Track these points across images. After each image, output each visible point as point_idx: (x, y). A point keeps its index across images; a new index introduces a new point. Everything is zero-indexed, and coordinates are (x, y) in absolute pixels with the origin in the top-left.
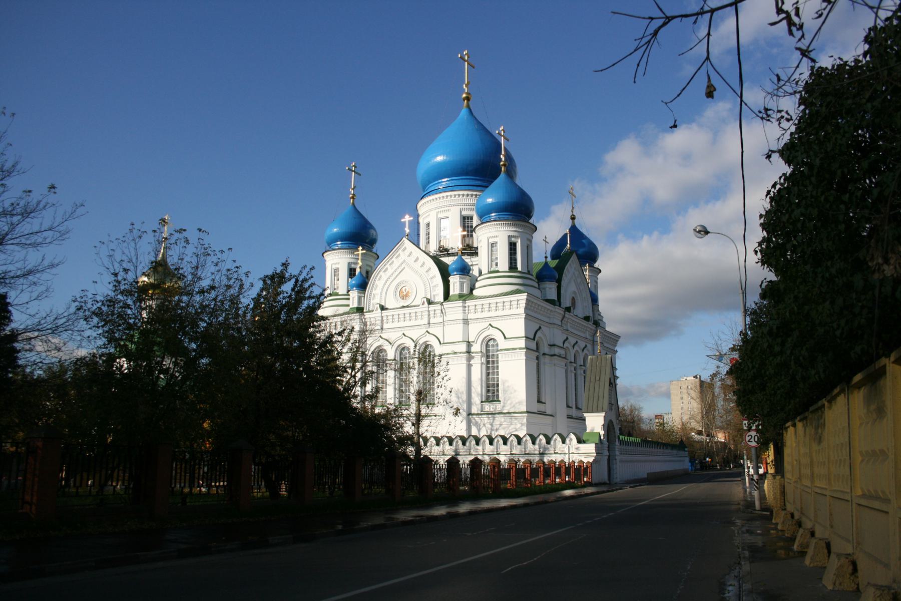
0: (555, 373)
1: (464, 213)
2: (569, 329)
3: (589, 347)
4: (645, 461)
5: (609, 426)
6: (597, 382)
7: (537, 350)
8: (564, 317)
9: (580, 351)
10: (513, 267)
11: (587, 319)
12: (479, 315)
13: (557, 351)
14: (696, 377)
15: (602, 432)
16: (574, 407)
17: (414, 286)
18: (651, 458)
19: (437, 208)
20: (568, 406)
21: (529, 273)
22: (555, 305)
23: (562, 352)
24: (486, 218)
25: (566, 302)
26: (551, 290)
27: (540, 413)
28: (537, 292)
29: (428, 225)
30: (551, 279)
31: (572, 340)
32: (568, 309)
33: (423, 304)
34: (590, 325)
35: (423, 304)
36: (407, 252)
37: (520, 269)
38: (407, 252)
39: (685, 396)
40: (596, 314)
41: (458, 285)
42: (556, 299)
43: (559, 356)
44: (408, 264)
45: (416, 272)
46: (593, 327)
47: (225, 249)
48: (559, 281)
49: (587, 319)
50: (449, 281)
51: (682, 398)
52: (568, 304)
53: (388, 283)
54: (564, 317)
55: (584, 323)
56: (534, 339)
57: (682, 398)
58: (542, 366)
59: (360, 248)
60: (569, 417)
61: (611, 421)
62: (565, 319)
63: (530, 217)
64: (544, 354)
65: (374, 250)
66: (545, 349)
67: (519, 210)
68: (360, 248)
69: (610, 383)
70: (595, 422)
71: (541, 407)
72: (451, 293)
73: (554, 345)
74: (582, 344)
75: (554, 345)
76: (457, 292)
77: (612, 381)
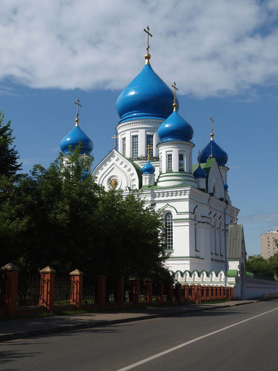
0: (204, 232)
3: (223, 217)
5: (241, 267)
8: (210, 199)
9: (218, 219)
10: (181, 170)
11: (221, 199)
12: (161, 198)
13: (205, 220)
16: (219, 255)
17: (120, 181)
18: (265, 286)
19: (132, 129)
20: (211, 253)
23: (209, 220)
24: (125, 116)
26: (202, 182)
27: (197, 257)
28: (195, 185)
30: (202, 176)
32: (212, 194)
33: (126, 190)
34: (223, 203)
35: (126, 190)
36: (116, 158)
37: (185, 171)
38: (116, 158)
40: (227, 196)
41: (147, 180)
42: (205, 189)
43: (207, 223)
48: (207, 178)
49: (221, 199)
52: (212, 192)
53: (105, 175)
54: (210, 199)
55: (220, 202)
56: (194, 213)
57: (269, 245)
58: (198, 229)
59: (85, 154)
61: (242, 263)
62: (210, 200)
64: (199, 222)
65: (91, 154)
66: (199, 219)
68: (85, 154)
69: (242, 241)
70: (234, 266)
71: (197, 254)
72: (144, 184)
73: (204, 217)
75: (204, 217)
76: (147, 184)
77: (243, 240)
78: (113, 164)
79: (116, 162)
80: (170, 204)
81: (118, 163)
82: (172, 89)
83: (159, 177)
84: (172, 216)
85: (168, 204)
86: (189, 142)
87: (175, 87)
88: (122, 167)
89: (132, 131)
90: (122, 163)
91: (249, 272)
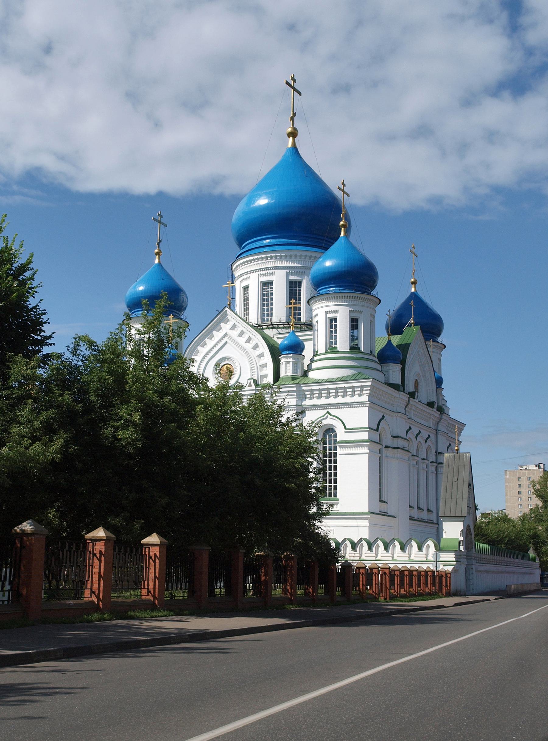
1: (292, 277)
2: (413, 417)
3: (433, 437)
4: (502, 572)
5: (466, 532)
6: (455, 483)
7: (381, 442)
8: (408, 404)
9: (423, 442)
10: (354, 348)
11: (431, 404)
12: (315, 402)
13: (400, 443)
14: (538, 466)
15: (461, 538)
16: (416, 507)
18: (504, 568)
20: (410, 507)
21: (371, 353)
22: (399, 390)
23: (405, 444)
25: (410, 388)
27: (384, 514)
28: (380, 376)
29: (246, 288)
31: (415, 430)
32: (412, 395)
33: (250, 385)
34: (434, 412)
36: (230, 324)
37: (362, 349)
38: (230, 324)
39: (524, 490)
40: (440, 398)
41: (290, 366)
44: (230, 338)
45: (242, 348)
46: (437, 414)
47: (519, 489)
48: (403, 363)
49: (431, 404)
50: (280, 360)
51: (520, 493)
52: (412, 390)
54: (408, 404)
55: (428, 409)
56: (377, 430)
57: (520, 493)
60: (412, 519)
61: (468, 526)
62: (409, 406)
63: (373, 287)
64: (386, 447)
66: (388, 440)
67: (357, 280)
69: (470, 485)
72: (282, 374)
74: (425, 434)
75: (398, 437)
77: (471, 483)
78: (226, 335)
79: (230, 333)
80: (331, 411)
81: (234, 334)
82: (339, 194)
83: (312, 361)
84: (335, 436)
85: (328, 412)
86: (370, 294)
87: (343, 191)
88: (242, 341)
89: (262, 272)
90: (241, 334)
91: (481, 543)
